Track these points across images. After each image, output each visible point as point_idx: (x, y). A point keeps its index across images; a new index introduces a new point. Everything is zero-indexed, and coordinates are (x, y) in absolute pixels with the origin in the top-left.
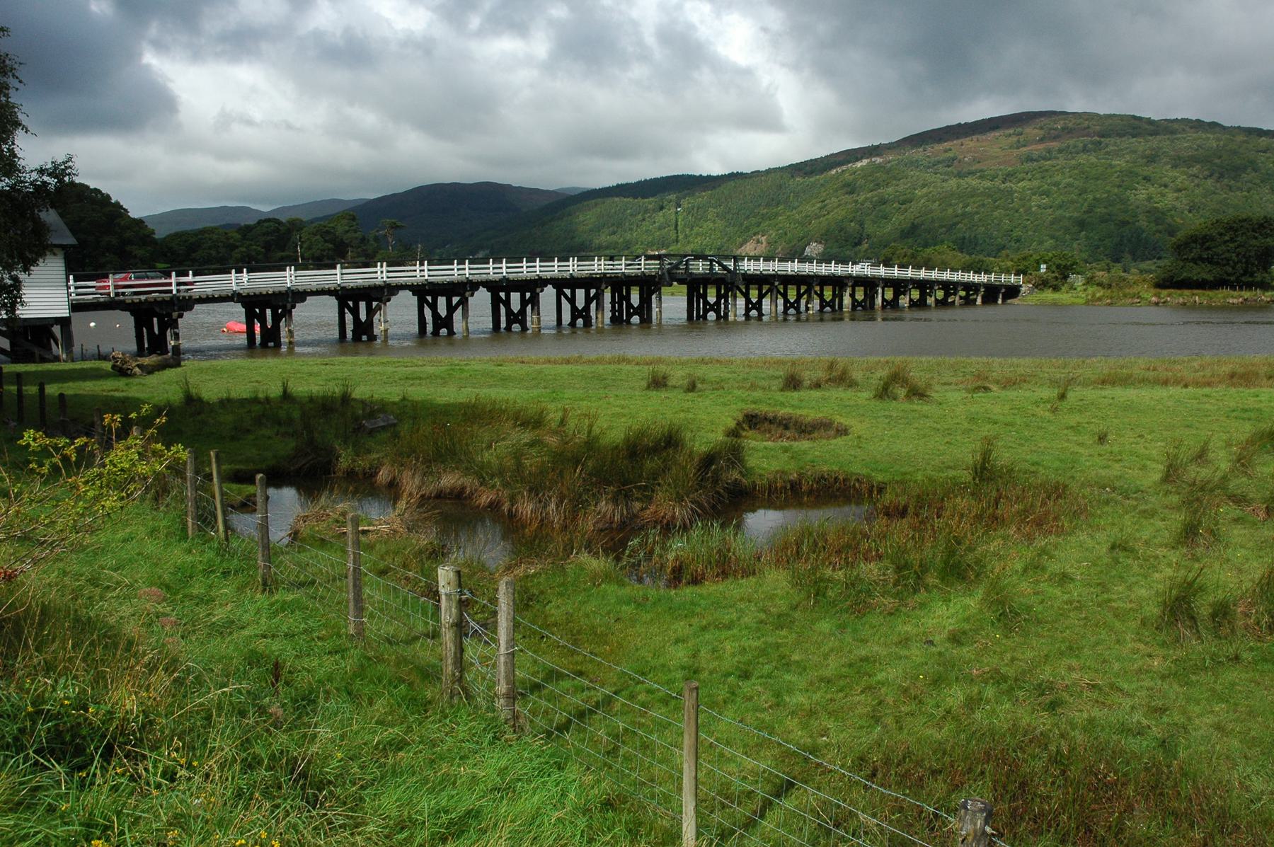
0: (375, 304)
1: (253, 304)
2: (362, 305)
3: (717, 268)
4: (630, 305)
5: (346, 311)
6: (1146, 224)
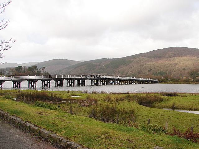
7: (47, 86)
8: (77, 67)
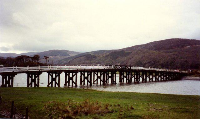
7: (72, 79)
8: (79, 57)
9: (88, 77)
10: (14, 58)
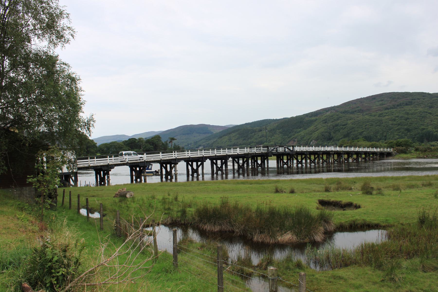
0: (173, 165)
1: (98, 170)
2: (168, 166)
3: (286, 149)
4: (257, 164)
5: (163, 168)
6: (431, 129)
9: (222, 167)
10: (124, 139)
